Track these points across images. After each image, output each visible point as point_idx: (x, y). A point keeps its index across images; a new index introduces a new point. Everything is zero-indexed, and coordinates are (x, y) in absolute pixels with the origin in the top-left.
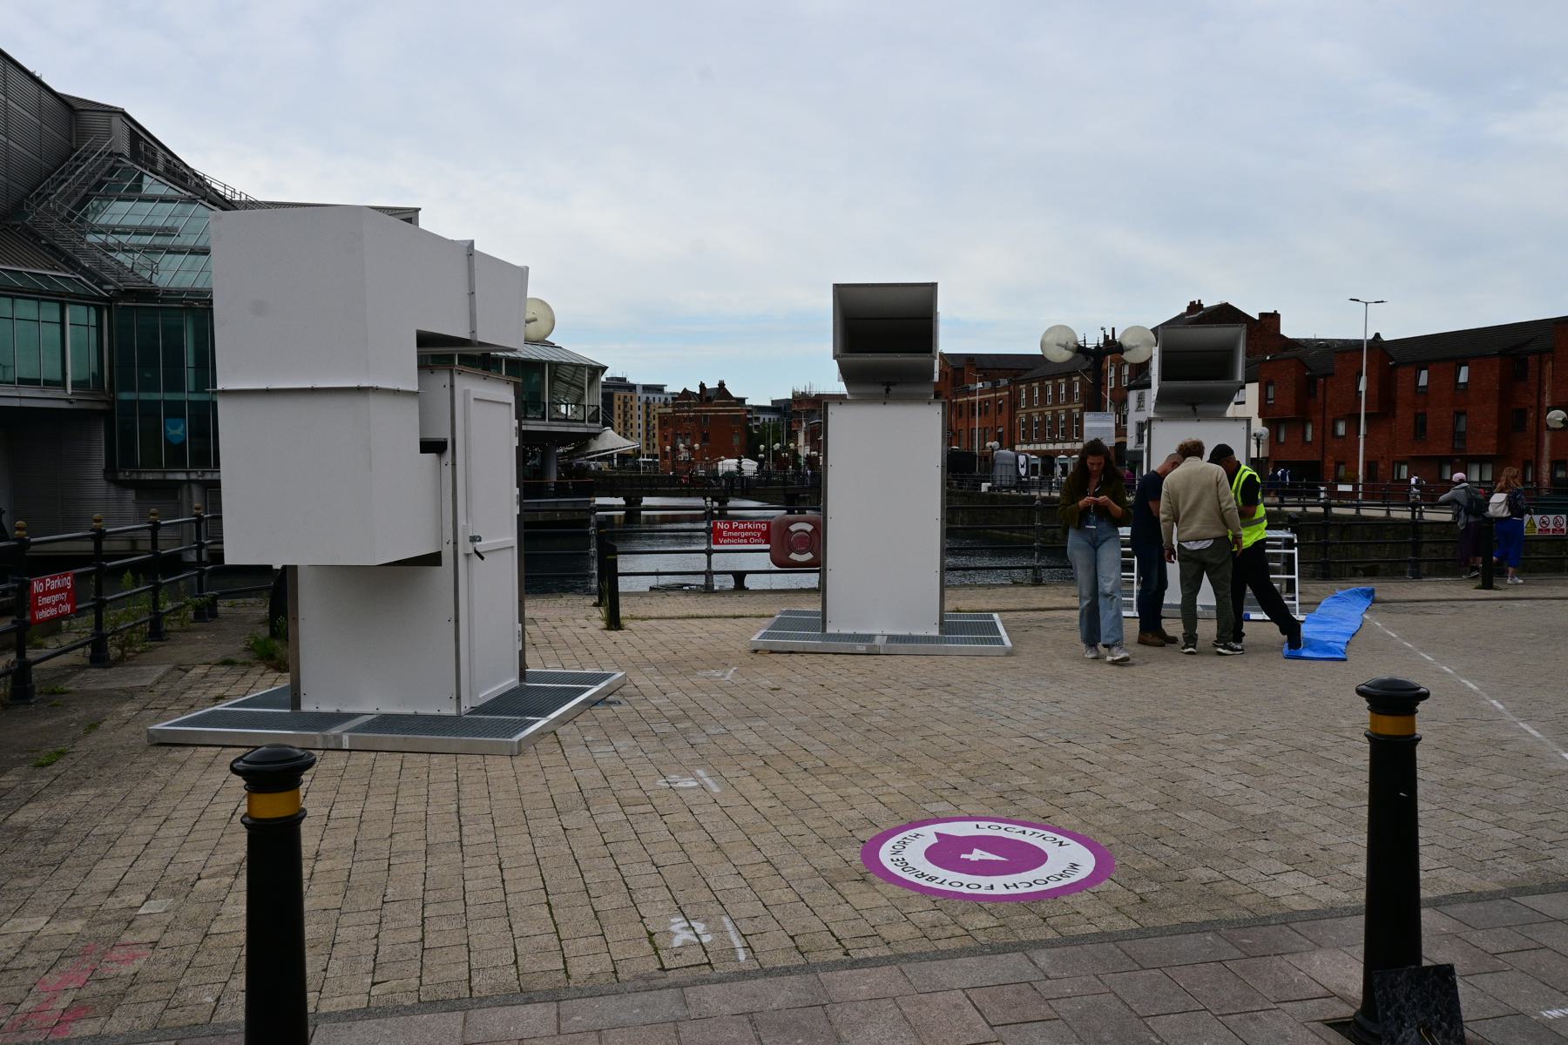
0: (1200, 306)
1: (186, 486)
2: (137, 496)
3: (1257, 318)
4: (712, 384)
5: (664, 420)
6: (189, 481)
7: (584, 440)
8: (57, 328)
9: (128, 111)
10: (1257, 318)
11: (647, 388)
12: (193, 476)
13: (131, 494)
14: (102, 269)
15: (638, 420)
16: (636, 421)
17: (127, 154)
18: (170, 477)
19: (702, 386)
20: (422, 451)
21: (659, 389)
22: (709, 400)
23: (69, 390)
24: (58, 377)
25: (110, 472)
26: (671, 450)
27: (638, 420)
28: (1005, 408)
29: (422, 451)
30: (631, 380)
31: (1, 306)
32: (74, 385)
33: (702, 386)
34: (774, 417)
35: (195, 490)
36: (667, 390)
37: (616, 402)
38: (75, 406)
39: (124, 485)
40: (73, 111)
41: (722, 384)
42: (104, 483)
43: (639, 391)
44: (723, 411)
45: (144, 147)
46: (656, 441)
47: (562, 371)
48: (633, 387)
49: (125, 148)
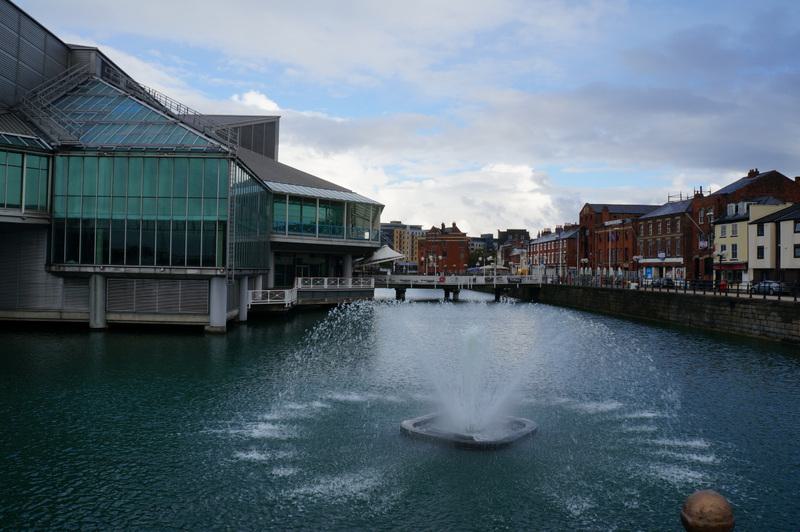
0: (757, 172)
1: (94, 276)
2: (65, 283)
3: (794, 179)
4: (449, 225)
5: (421, 244)
6: (96, 273)
7: (371, 251)
8: (20, 169)
9: (100, 49)
10: (794, 179)
11: (412, 227)
12: (98, 270)
13: (61, 281)
14: (51, 133)
15: (407, 242)
16: (406, 240)
17: (99, 74)
18: (83, 270)
19: (443, 225)
20: (762, 258)
21: (418, 228)
22: (446, 233)
23: (23, 211)
24: (18, 203)
25: (48, 264)
26: (443, 256)
27: (407, 242)
28: (630, 236)
29: (762, 258)
30: (404, 223)
31: (2, 155)
32: (27, 208)
33: (443, 225)
34: (482, 243)
35: (100, 280)
36: (423, 228)
37: (396, 234)
38: (26, 221)
39: (58, 274)
40: (70, 51)
41: (454, 224)
42: (45, 273)
43: (408, 228)
44: (449, 239)
45: (109, 69)
46: (416, 256)
47: (360, 211)
48: (405, 227)
49: (98, 71)
